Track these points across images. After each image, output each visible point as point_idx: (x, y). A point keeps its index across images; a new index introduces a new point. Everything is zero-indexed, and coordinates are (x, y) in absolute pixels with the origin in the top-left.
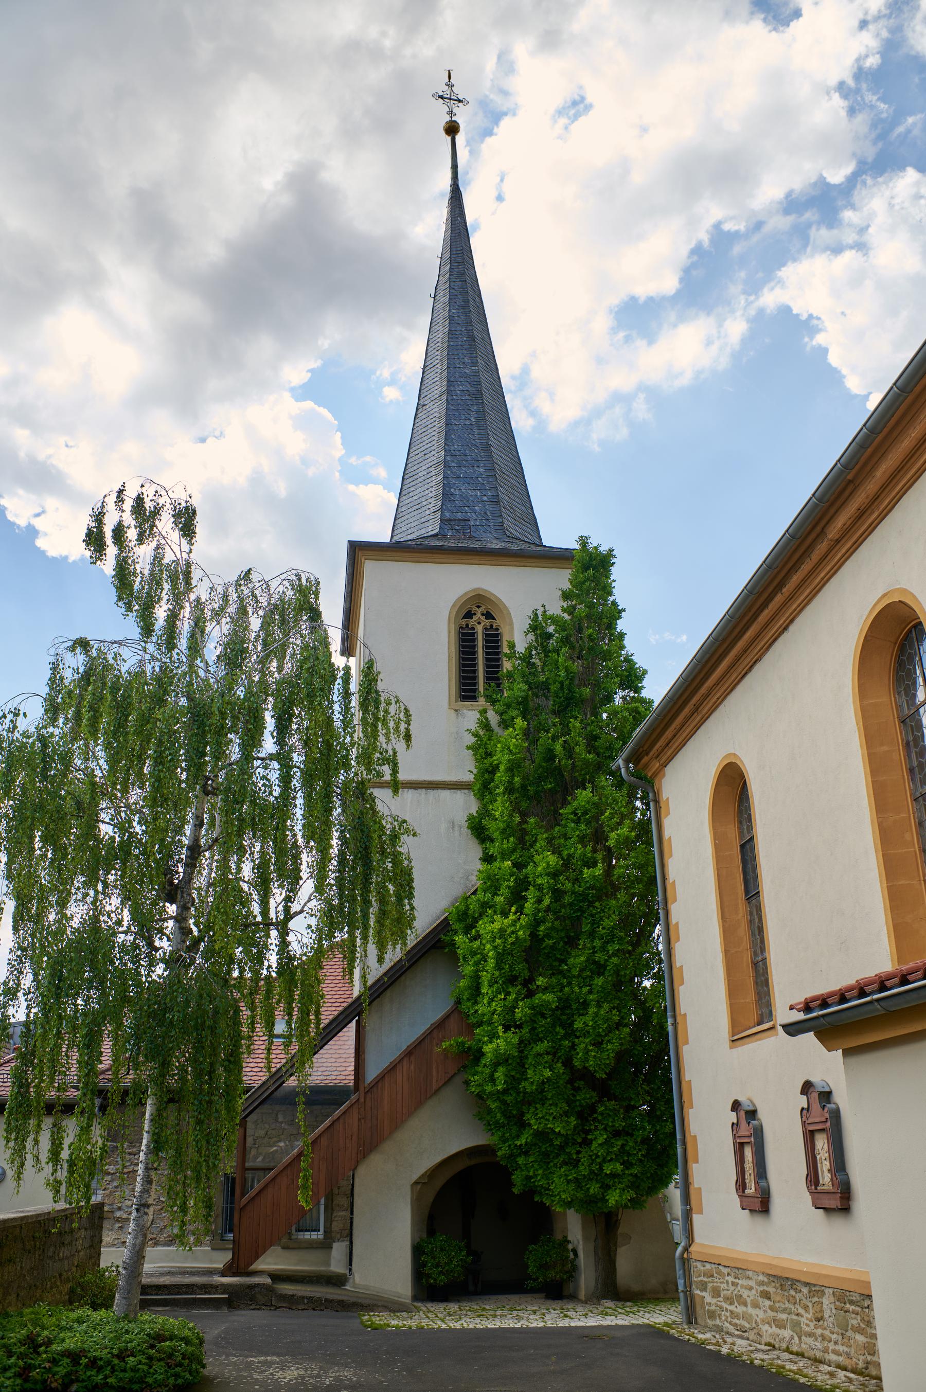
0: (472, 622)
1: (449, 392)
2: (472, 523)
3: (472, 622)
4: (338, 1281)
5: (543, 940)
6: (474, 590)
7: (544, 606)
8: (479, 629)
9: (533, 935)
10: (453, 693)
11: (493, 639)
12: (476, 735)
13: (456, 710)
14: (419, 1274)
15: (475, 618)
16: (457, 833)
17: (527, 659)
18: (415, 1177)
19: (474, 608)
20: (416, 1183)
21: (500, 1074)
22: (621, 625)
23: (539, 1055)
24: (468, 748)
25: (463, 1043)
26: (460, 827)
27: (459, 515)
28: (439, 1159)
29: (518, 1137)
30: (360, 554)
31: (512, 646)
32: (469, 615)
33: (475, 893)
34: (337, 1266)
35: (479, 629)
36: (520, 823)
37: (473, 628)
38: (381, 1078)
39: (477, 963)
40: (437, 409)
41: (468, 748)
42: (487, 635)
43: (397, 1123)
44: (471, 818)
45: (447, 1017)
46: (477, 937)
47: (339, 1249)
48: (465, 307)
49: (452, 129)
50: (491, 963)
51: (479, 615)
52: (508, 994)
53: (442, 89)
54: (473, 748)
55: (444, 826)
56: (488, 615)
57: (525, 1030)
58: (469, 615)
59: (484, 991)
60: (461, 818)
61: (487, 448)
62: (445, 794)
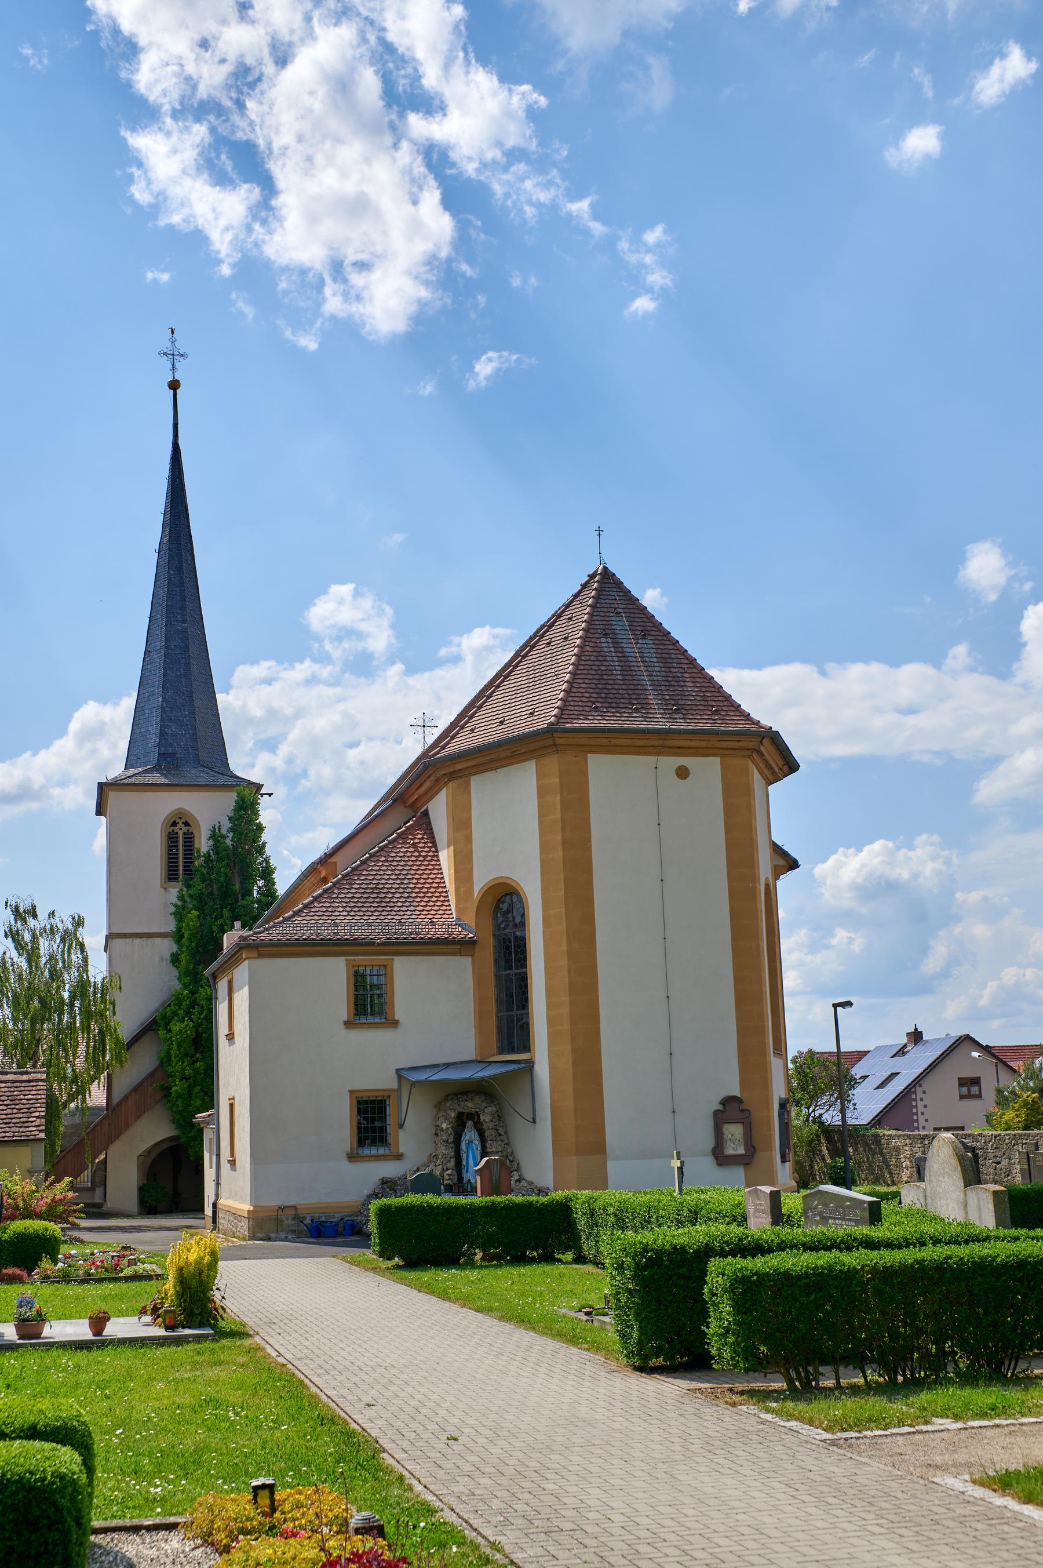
0: (176, 829)
1: (166, 647)
2: (178, 756)
3: (176, 829)
4: (99, 1206)
5: (202, 1034)
6: (177, 809)
7: (219, 823)
8: (181, 833)
9: (197, 1031)
10: (163, 877)
11: (189, 840)
12: (176, 906)
13: (165, 889)
14: (142, 1202)
15: (178, 826)
16: (164, 963)
17: (207, 856)
18: (139, 1153)
19: (178, 820)
20: (141, 1156)
21: (179, 1102)
22: (264, 837)
23: (197, 1093)
24: (171, 914)
25: (163, 1085)
26: (167, 960)
27: (170, 750)
28: (152, 1143)
29: (191, 1132)
30: (105, 788)
31: (199, 851)
32: (174, 824)
33: (169, 1005)
34: (98, 1200)
35: (181, 833)
36: (193, 969)
37: (177, 833)
38: (120, 1103)
39: (169, 1046)
40: (158, 658)
41: (171, 914)
42: (185, 838)
43: (127, 1126)
44: (173, 955)
45: (155, 1070)
46: (170, 1031)
47: (99, 1191)
48: (179, 569)
49: (174, 385)
50: (175, 1047)
51: (180, 824)
52: (183, 1062)
53: (166, 345)
54: (175, 914)
55: (157, 960)
56: (187, 824)
57: (191, 1081)
58: (174, 824)
59: (173, 1059)
60: (167, 955)
61: (190, 694)
62: (158, 940)
